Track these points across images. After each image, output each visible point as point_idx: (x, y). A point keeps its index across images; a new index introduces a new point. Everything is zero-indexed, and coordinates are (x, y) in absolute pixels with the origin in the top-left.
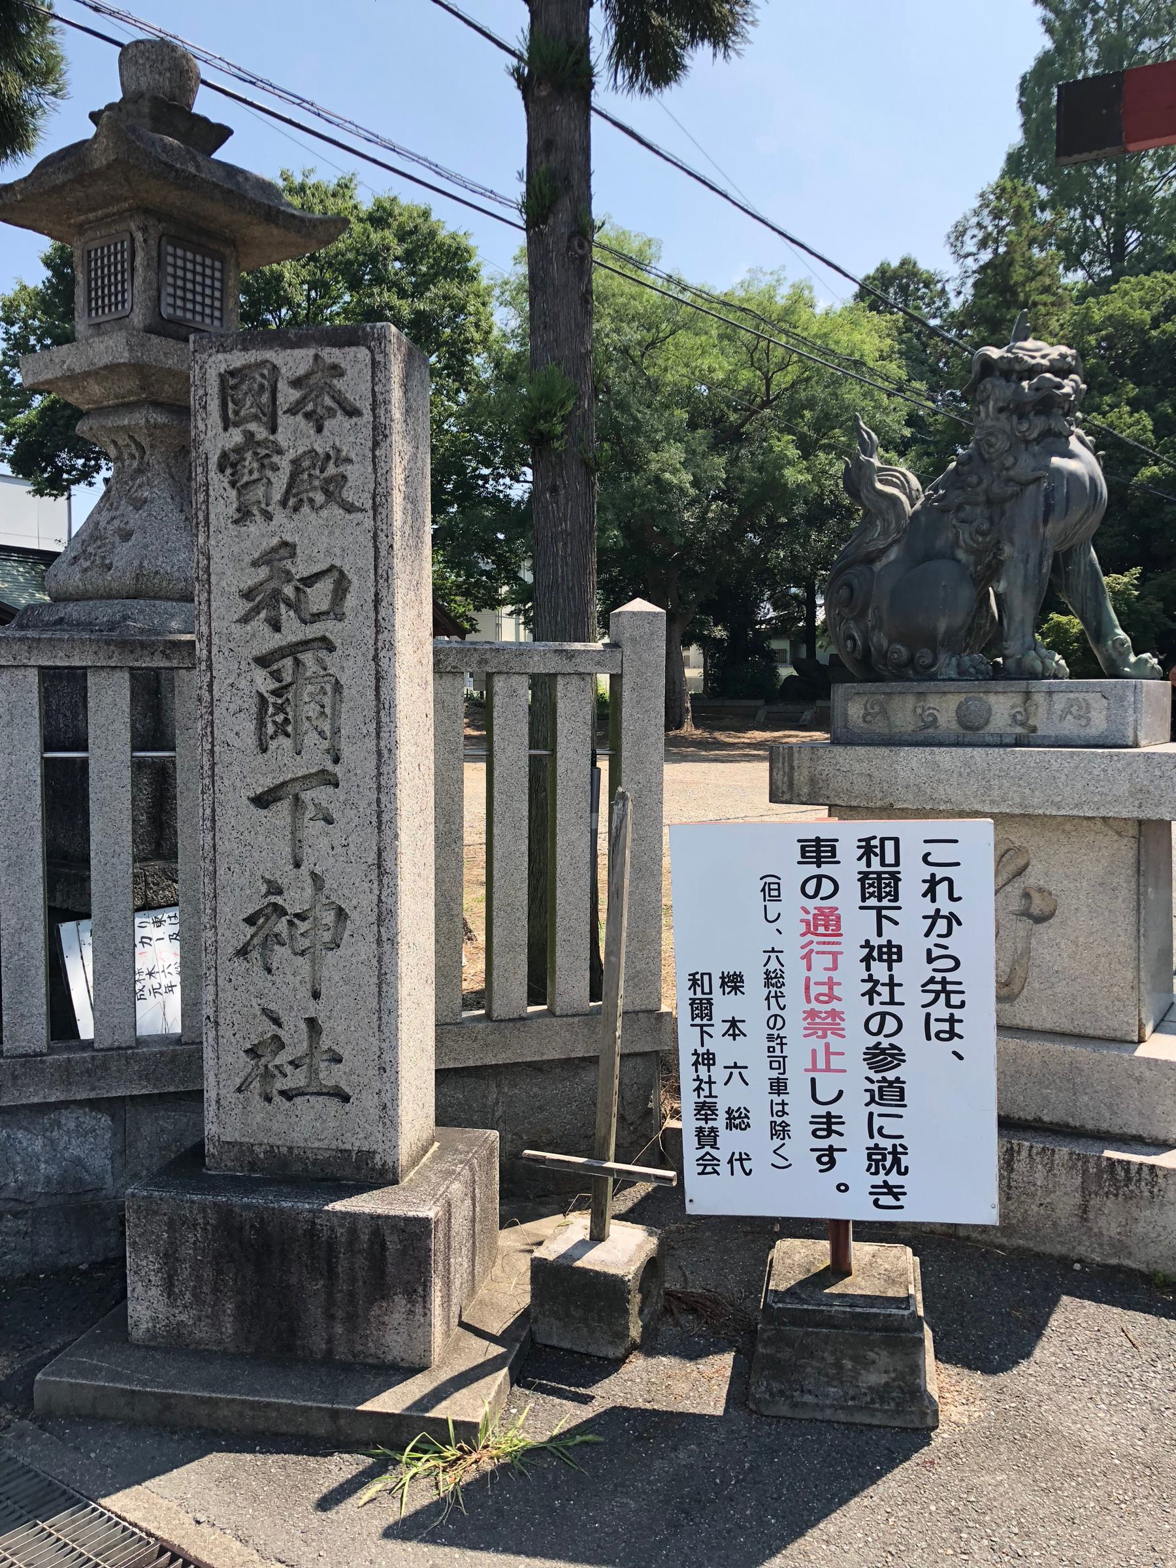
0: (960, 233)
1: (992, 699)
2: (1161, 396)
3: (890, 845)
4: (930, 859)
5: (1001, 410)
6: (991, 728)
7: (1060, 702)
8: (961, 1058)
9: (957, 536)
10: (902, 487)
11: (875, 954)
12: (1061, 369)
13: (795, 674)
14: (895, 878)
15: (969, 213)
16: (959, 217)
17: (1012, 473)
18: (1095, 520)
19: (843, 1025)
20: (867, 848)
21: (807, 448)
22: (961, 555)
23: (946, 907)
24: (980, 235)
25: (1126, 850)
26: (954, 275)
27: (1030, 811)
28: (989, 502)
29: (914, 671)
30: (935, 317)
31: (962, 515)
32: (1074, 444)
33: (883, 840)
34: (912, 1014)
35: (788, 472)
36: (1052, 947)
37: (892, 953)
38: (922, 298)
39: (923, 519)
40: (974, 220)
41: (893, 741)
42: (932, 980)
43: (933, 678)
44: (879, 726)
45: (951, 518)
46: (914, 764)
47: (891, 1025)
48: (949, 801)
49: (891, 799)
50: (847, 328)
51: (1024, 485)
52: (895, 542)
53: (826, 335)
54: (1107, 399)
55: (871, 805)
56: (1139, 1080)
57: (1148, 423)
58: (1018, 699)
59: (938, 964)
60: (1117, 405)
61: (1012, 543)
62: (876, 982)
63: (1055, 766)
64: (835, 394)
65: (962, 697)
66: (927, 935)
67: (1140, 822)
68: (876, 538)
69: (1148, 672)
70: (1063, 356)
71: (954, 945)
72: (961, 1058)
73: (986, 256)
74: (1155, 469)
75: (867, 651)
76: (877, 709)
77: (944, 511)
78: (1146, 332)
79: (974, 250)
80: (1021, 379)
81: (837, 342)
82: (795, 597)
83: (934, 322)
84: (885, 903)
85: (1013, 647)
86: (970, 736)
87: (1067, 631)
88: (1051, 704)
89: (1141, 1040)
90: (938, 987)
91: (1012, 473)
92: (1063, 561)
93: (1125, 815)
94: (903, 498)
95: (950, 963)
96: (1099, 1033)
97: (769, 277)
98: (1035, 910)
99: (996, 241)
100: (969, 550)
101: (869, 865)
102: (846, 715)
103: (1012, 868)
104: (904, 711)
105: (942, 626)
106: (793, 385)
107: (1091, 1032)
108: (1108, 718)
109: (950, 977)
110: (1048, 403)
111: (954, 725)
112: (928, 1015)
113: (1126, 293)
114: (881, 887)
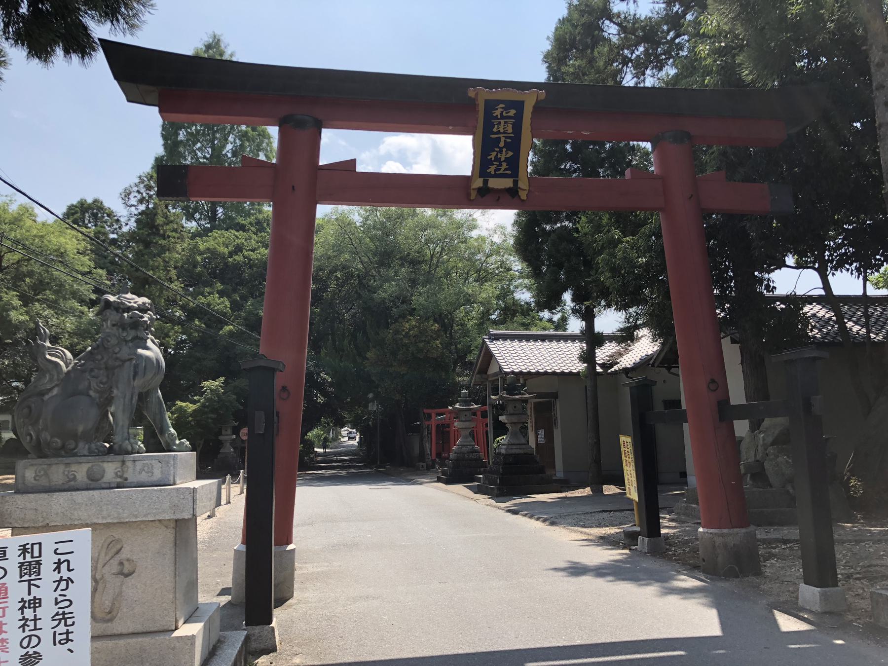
0: (127, 194)
1: (105, 465)
2: (235, 290)
3: (36, 547)
4: (58, 552)
5: (114, 325)
6: (105, 480)
7: (139, 465)
8: (72, 651)
9: (90, 383)
10: (61, 358)
11: (27, 605)
12: (143, 309)
13: (14, 437)
14: (39, 563)
15: (133, 185)
16: (127, 186)
17: (118, 355)
18: (160, 378)
19: (8, 646)
20: (24, 550)
21: (26, 300)
22: (92, 393)
23: (65, 574)
24: (139, 196)
25: (170, 534)
26: (126, 214)
27: (122, 520)
28: (106, 368)
29: (65, 452)
30: (113, 233)
31: (93, 374)
32: (149, 343)
33: (32, 545)
34: (46, 634)
35: (13, 314)
36: (133, 588)
37: (36, 603)
38: (106, 222)
39: (72, 375)
40: (136, 189)
41: (50, 490)
42: (57, 614)
43: (75, 455)
44: (44, 482)
45: (87, 376)
46: (61, 501)
47: (34, 641)
48: (80, 519)
49: (47, 521)
50: (57, 234)
51: (124, 361)
52: (57, 385)
53: (42, 237)
54: (207, 289)
55: (36, 525)
56: (173, 649)
57: (228, 303)
58: (119, 465)
59: (60, 605)
60: (212, 293)
61: (117, 388)
62: (27, 620)
63: (135, 497)
64: (47, 271)
65: (89, 465)
66: (55, 591)
67: (176, 521)
68: (46, 382)
69: (184, 449)
70: (144, 304)
71: (69, 594)
72: (72, 651)
73: (142, 207)
74: (231, 327)
75: (39, 442)
76: (42, 473)
77: (83, 371)
78: (226, 259)
79: (135, 203)
80: (124, 312)
81: (49, 241)
82: (16, 388)
83: (112, 236)
84: (33, 577)
85: (117, 439)
86: (94, 484)
87: (186, 411)
88: (135, 466)
89: (176, 629)
90: (61, 617)
91: (118, 355)
92: (143, 397)
93: (167, 518)
94: (62, 363)
95: (68, 603)
96: (156, 629)
97: (4, 198)
98: (126, 571)
99: (148, 201)
100: (96, 391)
101: (24, 558)
102: (24, 477)
103: (114, 550)
104: (58, 472)
105: (81, 429)
106: (18, 262)
107: (152, 629)
108: (162, 472)
109: (67, 610)
110: (136, 324)
111: (85, 479)
112: (55, 632)
113: (216, 238)
114: (30, 569)
